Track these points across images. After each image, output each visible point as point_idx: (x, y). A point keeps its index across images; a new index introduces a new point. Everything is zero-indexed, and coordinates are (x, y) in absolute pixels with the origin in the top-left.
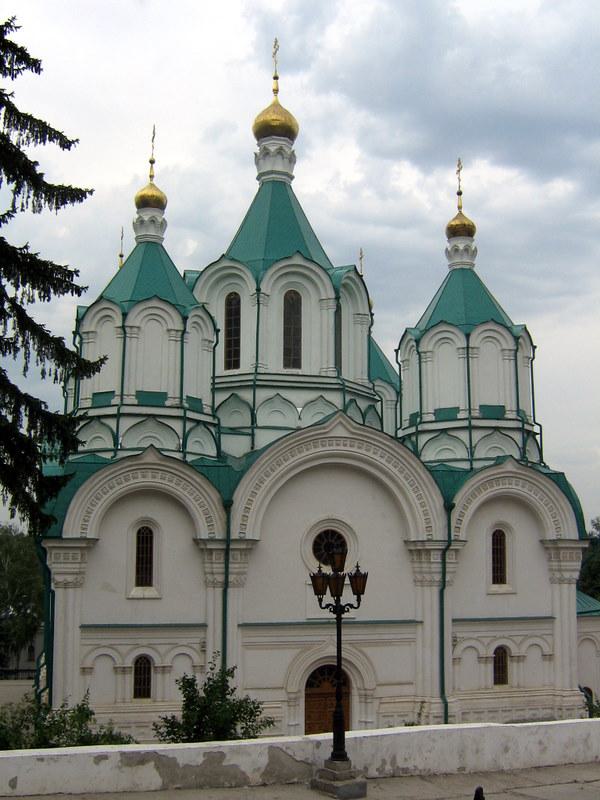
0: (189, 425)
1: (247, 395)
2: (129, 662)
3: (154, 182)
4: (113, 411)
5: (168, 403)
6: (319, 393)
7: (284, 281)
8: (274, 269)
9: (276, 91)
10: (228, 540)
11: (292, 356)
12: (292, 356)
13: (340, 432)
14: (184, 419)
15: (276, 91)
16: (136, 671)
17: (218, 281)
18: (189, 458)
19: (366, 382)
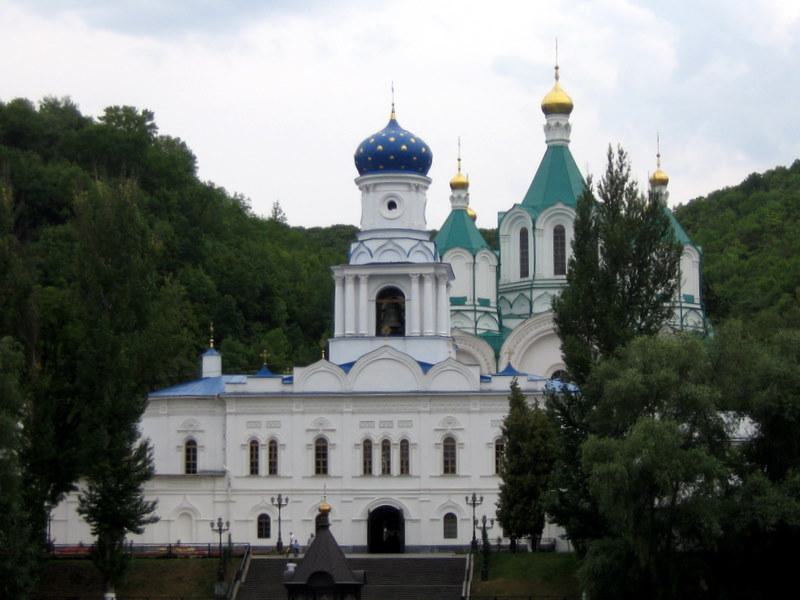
0: (478, 315)
1: (528, 294)
2: (360, 442)
5: (467, 303)
6: (375, 260)
7: (553, 219)
8: (547, 211)
14: (475, 311)
17: (549, 218)
18: (478, 332)
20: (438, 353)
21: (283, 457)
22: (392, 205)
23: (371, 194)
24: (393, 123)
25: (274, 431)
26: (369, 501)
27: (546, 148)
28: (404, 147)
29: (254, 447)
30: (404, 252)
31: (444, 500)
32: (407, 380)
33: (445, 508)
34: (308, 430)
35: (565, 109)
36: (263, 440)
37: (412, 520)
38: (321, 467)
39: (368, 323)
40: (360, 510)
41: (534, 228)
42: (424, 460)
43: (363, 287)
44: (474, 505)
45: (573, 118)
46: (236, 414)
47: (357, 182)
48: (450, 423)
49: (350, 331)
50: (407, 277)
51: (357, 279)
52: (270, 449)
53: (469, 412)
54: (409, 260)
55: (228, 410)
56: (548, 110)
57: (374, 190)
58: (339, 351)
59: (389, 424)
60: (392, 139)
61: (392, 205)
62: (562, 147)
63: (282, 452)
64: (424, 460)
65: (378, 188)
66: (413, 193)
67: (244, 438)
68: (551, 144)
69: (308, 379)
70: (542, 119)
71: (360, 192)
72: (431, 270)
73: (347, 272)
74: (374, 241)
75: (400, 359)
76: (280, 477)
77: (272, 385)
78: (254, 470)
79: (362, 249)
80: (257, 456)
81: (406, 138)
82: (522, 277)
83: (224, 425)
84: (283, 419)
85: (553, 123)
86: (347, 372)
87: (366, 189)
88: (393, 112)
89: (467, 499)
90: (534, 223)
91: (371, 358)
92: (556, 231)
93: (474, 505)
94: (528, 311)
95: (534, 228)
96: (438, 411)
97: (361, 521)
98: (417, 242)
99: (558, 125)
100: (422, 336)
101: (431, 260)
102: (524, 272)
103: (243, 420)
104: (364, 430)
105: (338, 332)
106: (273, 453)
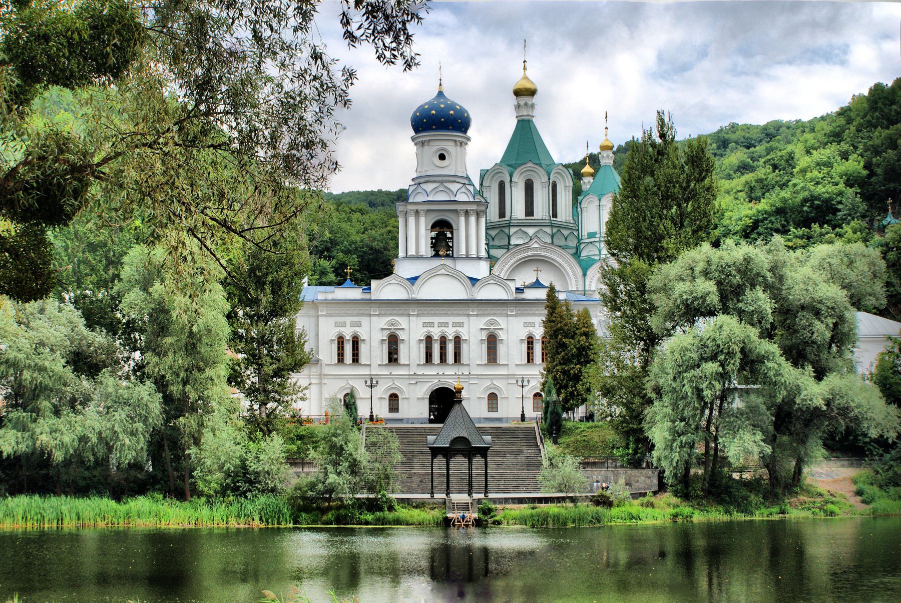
1: (506, 230)
3: (608, 137)
4: (598, 239)
6: (430, 198)
7: (524, 175)
8: (520, 168)
9: (525, 69)
10: (585, 291)
11: (529, 211)
12: (529, 211)
13: (536, 245)
15: (525, 69)
16: (389, 342)
17: (493, 177)
19: (572, 221)
20: (481, 270)
21: (363, 349)
22: (442, 157)
23: (426, 148)
24: (441, 94)
25: (357, 329)
26: (430, 384)
27: (515, 122)
28: (452, 112)
29: (341, 341)
30: (453, 192)
31: (342, 383)
32: (454, 291)
33: (342, 391)
34: (383, 329)
35: (532, 93)
36: (348, 337)
37: (361, 398)
38: (393, 358)
39: (425, 248)
40: (424, 391)
41: (511, 181)
42: (474, 352)
43: (422, 220)
44: (371, 387)
45: (536, 99)
46: (326, 316)
47: (413, 139)
48: (492, 324)
49: (412, 252)
50: (455, 211)
51: (417, 212)
52: (528, 343)
53: (507, 316)
54: (456, 199)
55: (320, 313)
56: (518, 93)
57: (428, 145)
58: (403, 269)
59: (446, 324)
60: (442, 106)
61: (442, 157)
62: (529, 120)
63: (363, 345)
64: (474, 352)
65: (431, 143)
66: (458, 147)
67: (333, 333)
68: (520, 118)
69: (382, 289)
70: (513, 100)
71: (415, 148)
72: (474, 207)
73: (409, 207)
74: (429, 184)
75: (455, 275)
76: (361, 364)
77: (351, 293)
78: (341, 358)
79: (420, 190)
80: (445, 349)
81: (452, 106)
82: (500, 217)
83: (317, 325)
84: (365, 321)
85: (522, 103)
86: (413, 284)
87: (421, 144)
88: (440, 85)
89: (366, 382)
90: (511, 177)
91: (432, 274)
92: (526, 184)
93: (371, 387)
94: (507, 244)
95: (511, 181)
96: (484, 315)
97: (423, 398)
98: (461, 185)
99: (526, 104)
100: (468, 257)
101: (472, 199)
102: (502, 214)
103: (332, 321)
104: (426, 329)
105: (401, 253)
106: (340, 346)
